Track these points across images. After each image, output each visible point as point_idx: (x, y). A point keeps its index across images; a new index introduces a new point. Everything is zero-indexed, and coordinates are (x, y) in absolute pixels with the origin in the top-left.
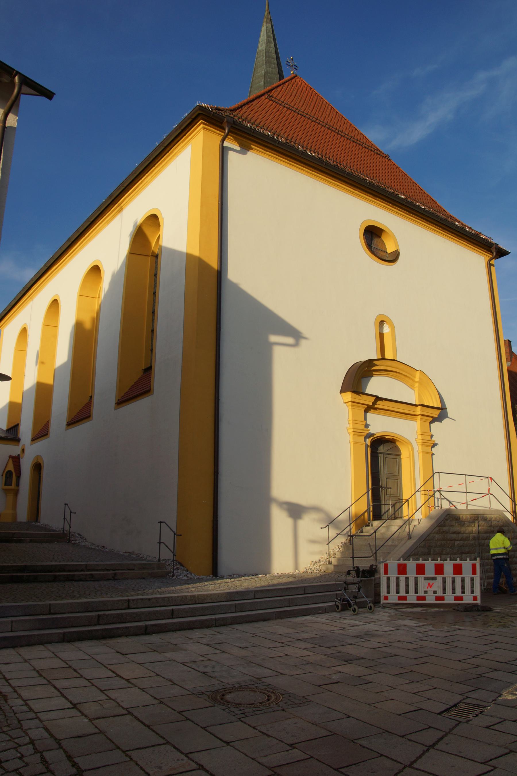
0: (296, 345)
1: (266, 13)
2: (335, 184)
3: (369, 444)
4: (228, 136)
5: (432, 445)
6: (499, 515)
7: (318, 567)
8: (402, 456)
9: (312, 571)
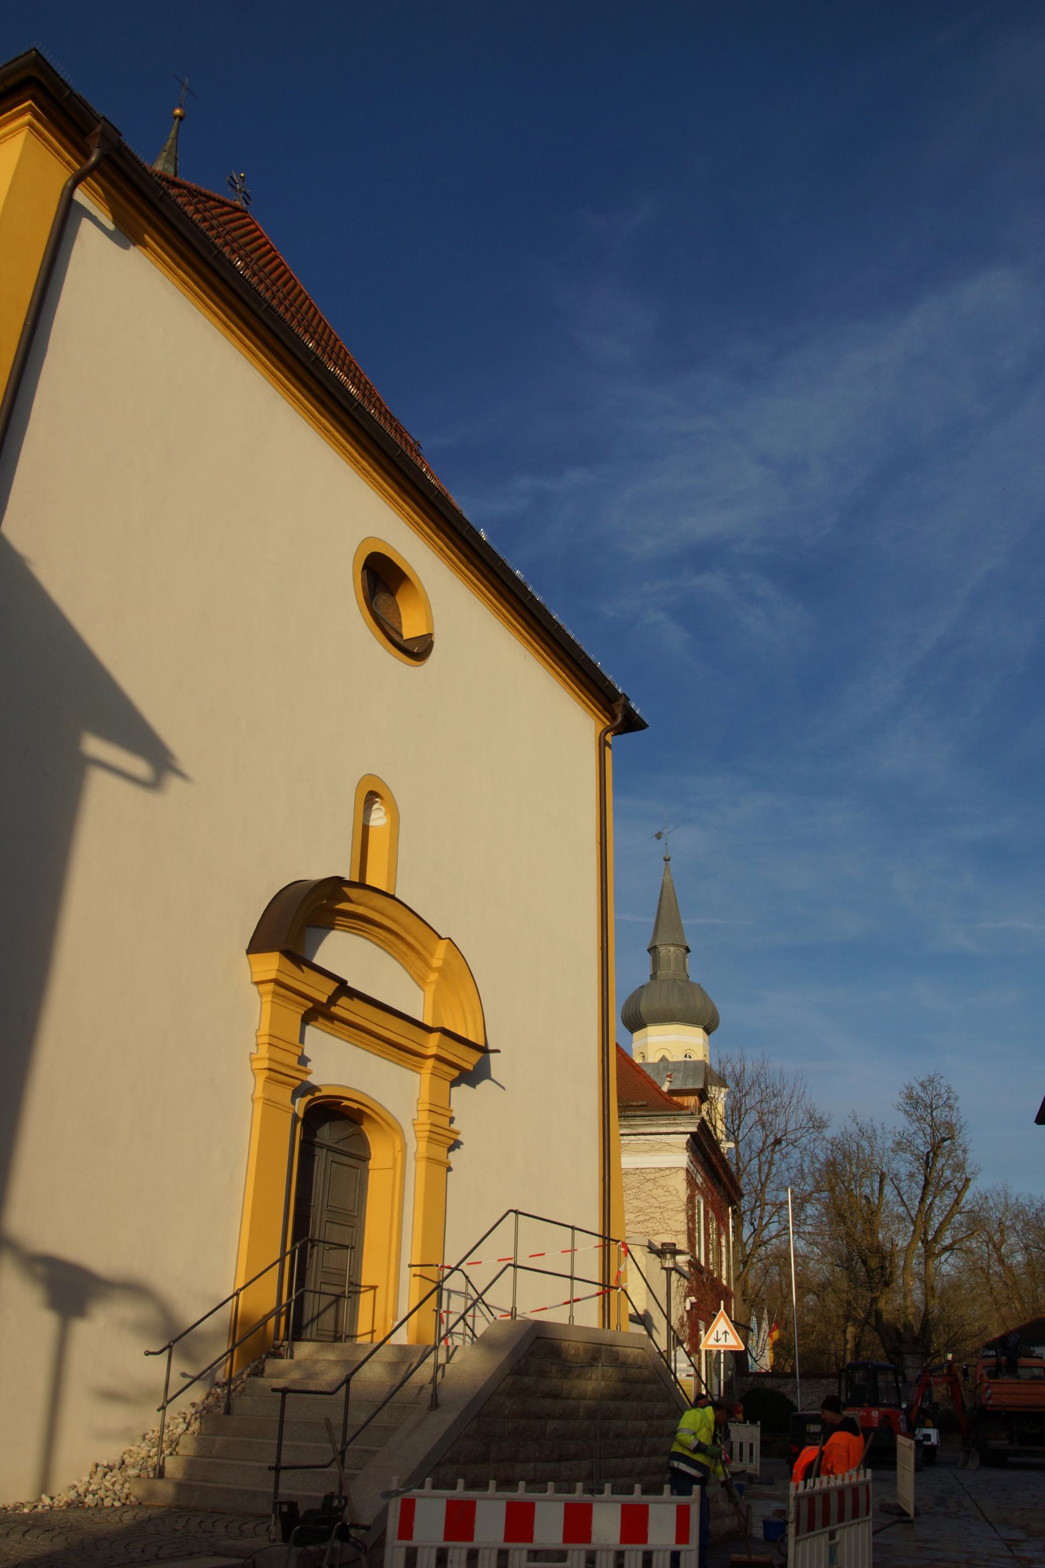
0: (154, 785)
1: (169, 143)
2: (320, 424)
3: (301, 1115)
4: (89, 179)
5: (452, 1142)
6: (643, 1349)
7: (117, 1487)
8: (371, 1164)
9: (100, 1502)
